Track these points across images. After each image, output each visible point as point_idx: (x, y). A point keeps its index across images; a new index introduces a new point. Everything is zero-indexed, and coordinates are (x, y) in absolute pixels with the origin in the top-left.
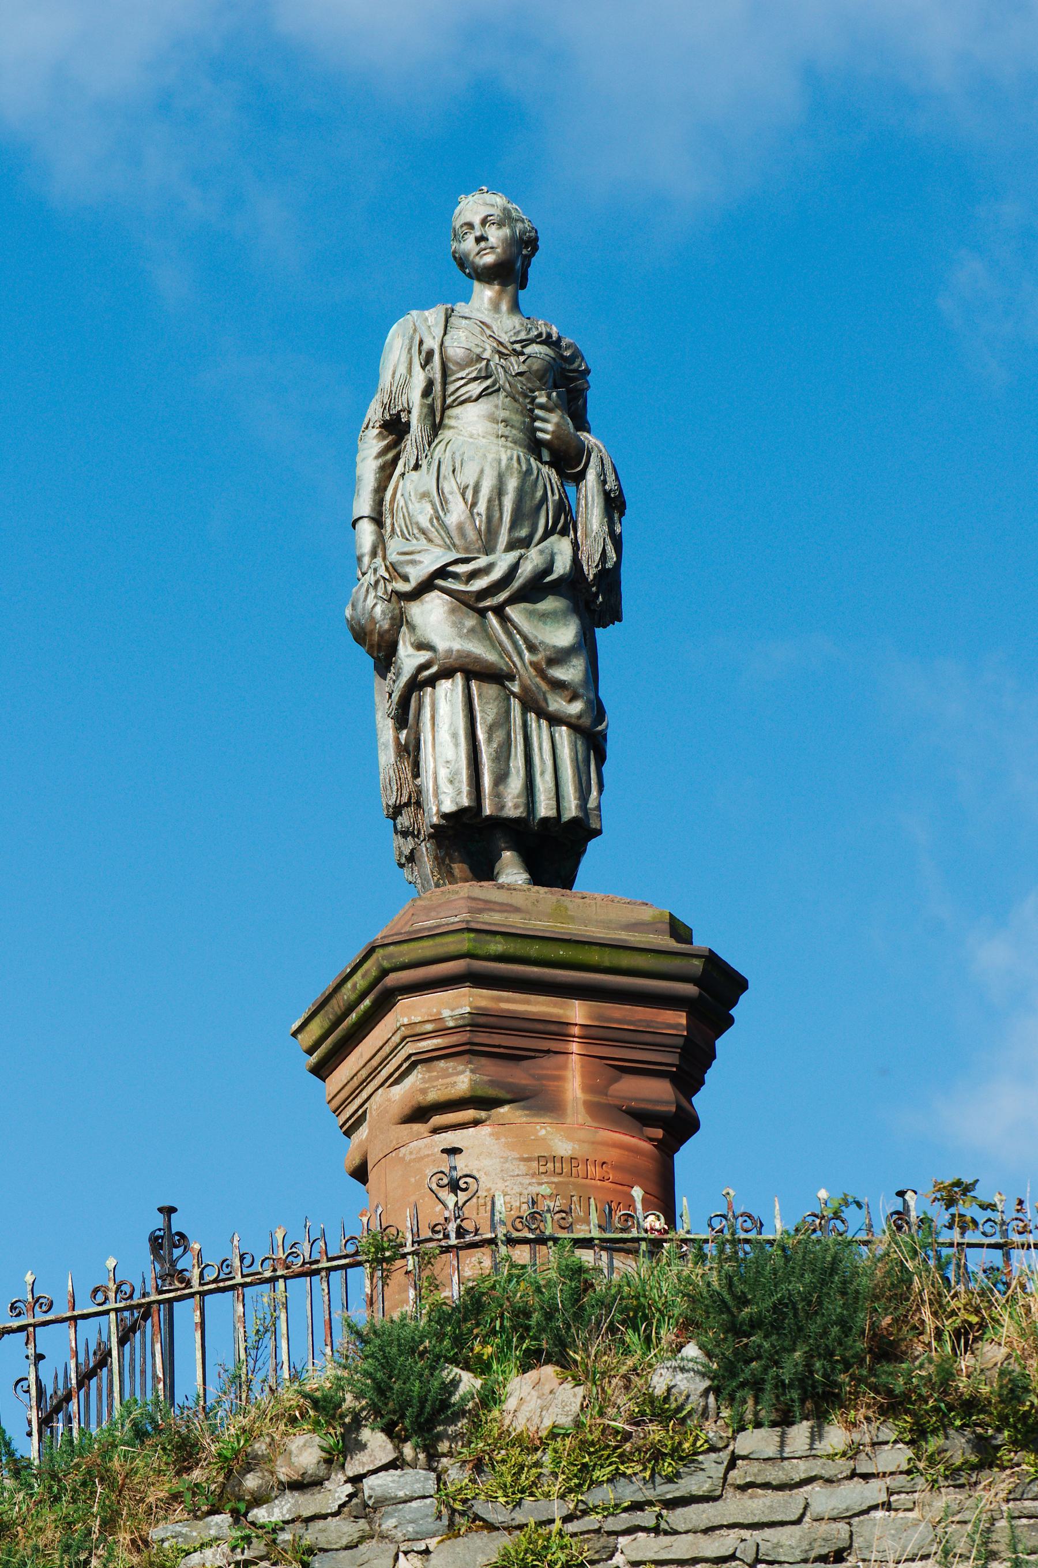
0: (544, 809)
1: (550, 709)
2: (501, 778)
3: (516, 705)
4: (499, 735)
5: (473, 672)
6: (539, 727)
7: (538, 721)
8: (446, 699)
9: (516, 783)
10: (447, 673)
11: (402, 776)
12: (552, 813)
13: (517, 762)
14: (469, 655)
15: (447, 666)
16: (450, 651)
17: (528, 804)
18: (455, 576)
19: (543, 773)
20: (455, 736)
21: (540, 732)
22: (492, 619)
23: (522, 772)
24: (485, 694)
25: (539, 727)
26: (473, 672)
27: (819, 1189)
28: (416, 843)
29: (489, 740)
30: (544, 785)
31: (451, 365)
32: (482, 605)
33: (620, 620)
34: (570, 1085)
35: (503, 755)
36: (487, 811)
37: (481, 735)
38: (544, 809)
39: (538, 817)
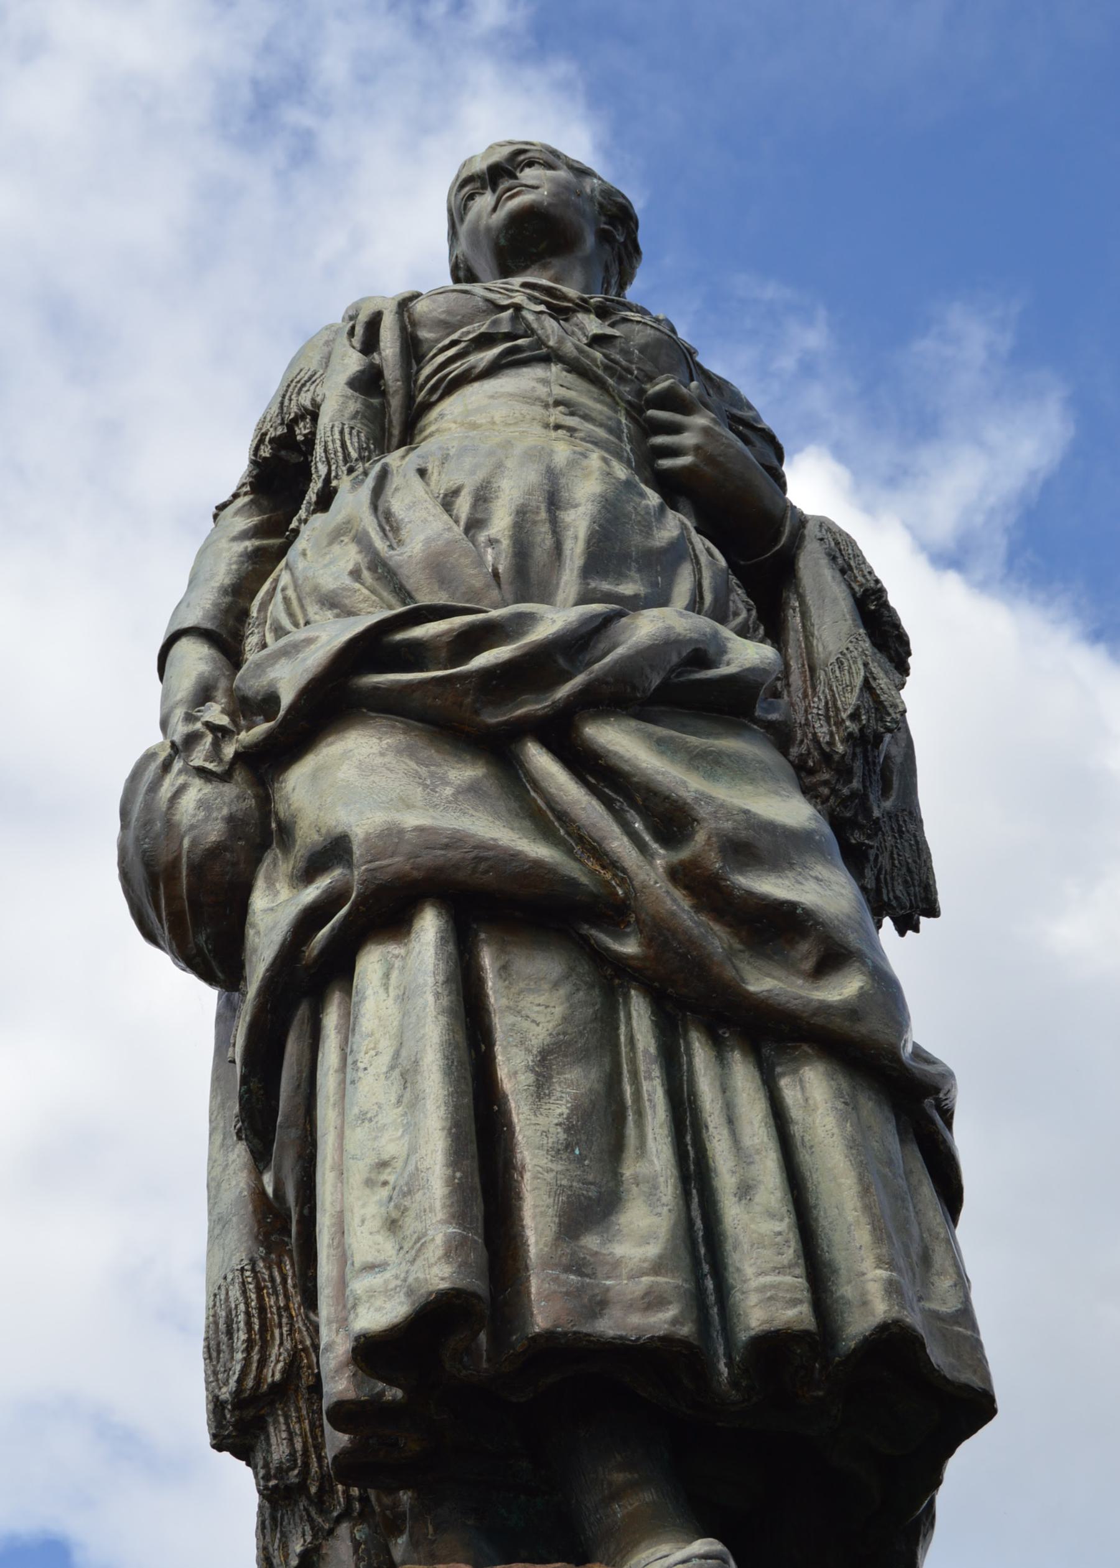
0: (765, 1293)
1: (752, 988)
2: (590, 1209)
3: (639, 1021)
4: (574, 1084)
5: (484, 905)
6: (725, 1088)
7: (721, 1059)
8: (398, 988)
9: (642, 1233)
10: (385, 912)
11: (270, 1301)
12: (796, 1314)
13: (653, 1156)
14: (456, 840)
15: (383, 877)
16: (392, 834)
17: (699, 1293)
18: (414, 656)
19: (745, 1191)
20: (406, 1074)
21: (729, 1089)
22: (541, 761)
23: (668, 1190)
24: (531, 1005)
25: (725, 1088)
26: (484, 905)
27: (406, 1488)
28: (316, 1531)
29: (541, 1088)
30: (755, 1227)
31: (424, 334)
32: (493, 718)
33: (933, 911)
34: (724, 936)
35: (603, 1128)
36: (544, 1307)
37: (512, 1070)
38: (765, 1293)
39: (743, 1336)
